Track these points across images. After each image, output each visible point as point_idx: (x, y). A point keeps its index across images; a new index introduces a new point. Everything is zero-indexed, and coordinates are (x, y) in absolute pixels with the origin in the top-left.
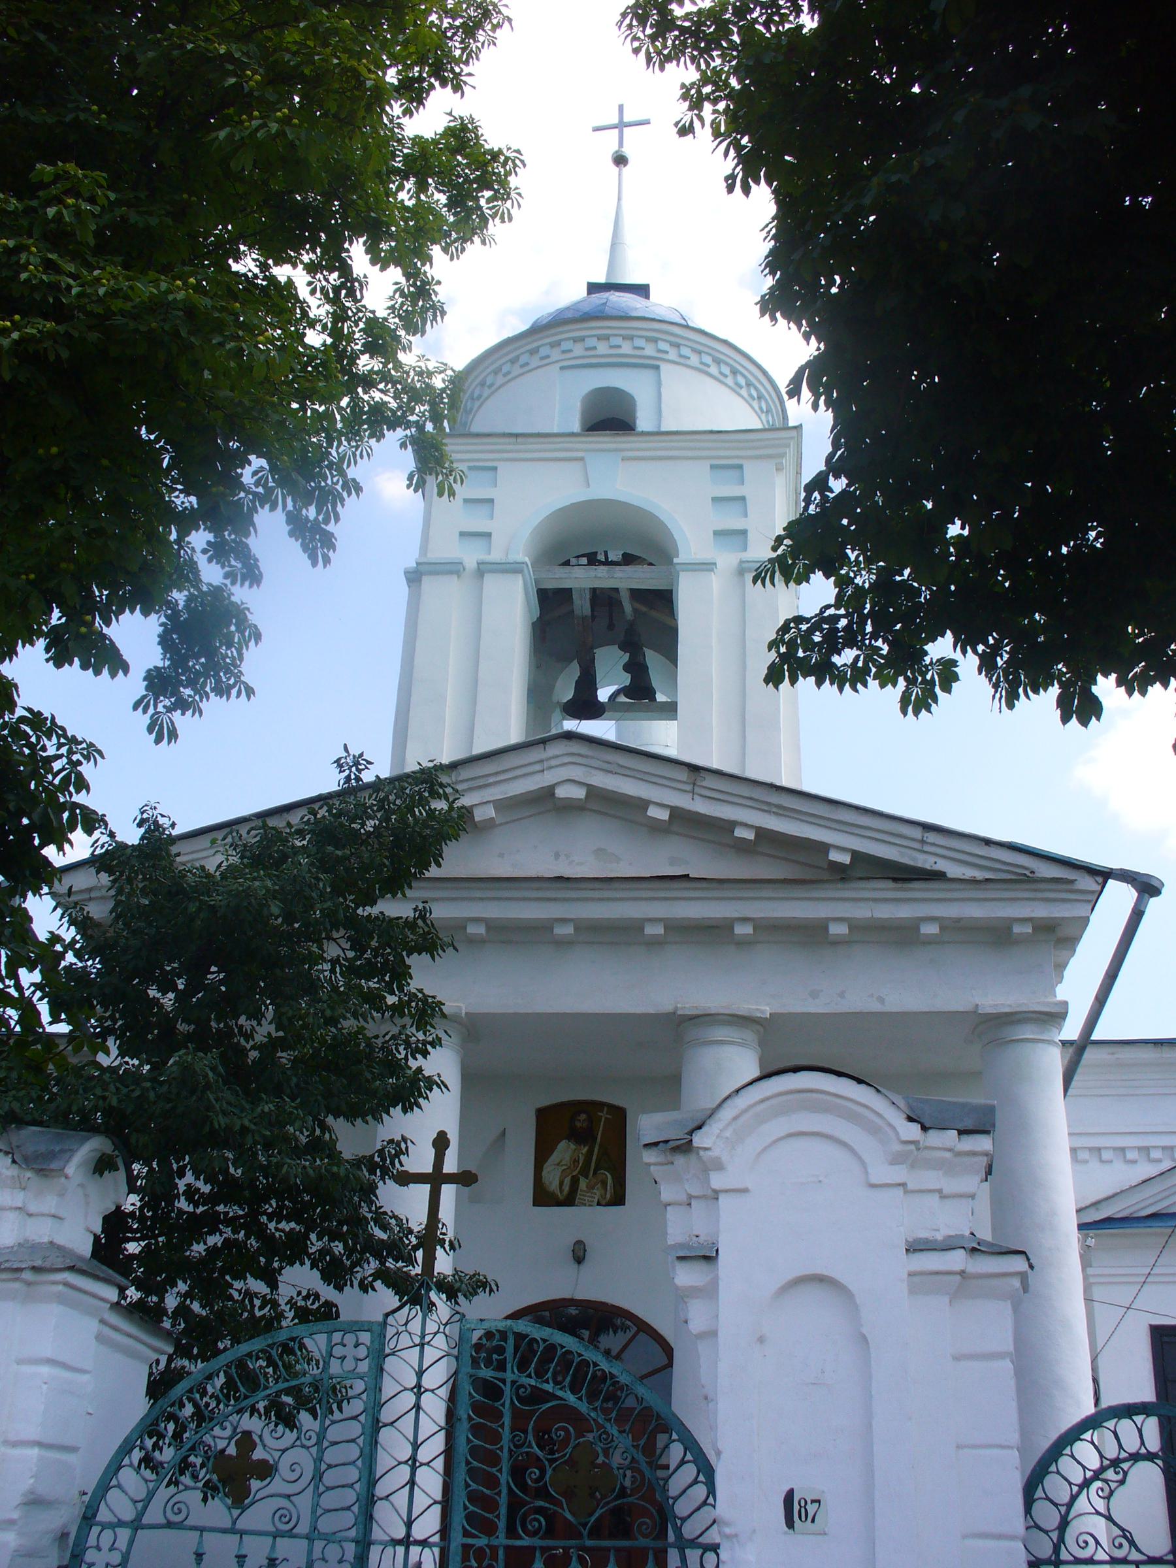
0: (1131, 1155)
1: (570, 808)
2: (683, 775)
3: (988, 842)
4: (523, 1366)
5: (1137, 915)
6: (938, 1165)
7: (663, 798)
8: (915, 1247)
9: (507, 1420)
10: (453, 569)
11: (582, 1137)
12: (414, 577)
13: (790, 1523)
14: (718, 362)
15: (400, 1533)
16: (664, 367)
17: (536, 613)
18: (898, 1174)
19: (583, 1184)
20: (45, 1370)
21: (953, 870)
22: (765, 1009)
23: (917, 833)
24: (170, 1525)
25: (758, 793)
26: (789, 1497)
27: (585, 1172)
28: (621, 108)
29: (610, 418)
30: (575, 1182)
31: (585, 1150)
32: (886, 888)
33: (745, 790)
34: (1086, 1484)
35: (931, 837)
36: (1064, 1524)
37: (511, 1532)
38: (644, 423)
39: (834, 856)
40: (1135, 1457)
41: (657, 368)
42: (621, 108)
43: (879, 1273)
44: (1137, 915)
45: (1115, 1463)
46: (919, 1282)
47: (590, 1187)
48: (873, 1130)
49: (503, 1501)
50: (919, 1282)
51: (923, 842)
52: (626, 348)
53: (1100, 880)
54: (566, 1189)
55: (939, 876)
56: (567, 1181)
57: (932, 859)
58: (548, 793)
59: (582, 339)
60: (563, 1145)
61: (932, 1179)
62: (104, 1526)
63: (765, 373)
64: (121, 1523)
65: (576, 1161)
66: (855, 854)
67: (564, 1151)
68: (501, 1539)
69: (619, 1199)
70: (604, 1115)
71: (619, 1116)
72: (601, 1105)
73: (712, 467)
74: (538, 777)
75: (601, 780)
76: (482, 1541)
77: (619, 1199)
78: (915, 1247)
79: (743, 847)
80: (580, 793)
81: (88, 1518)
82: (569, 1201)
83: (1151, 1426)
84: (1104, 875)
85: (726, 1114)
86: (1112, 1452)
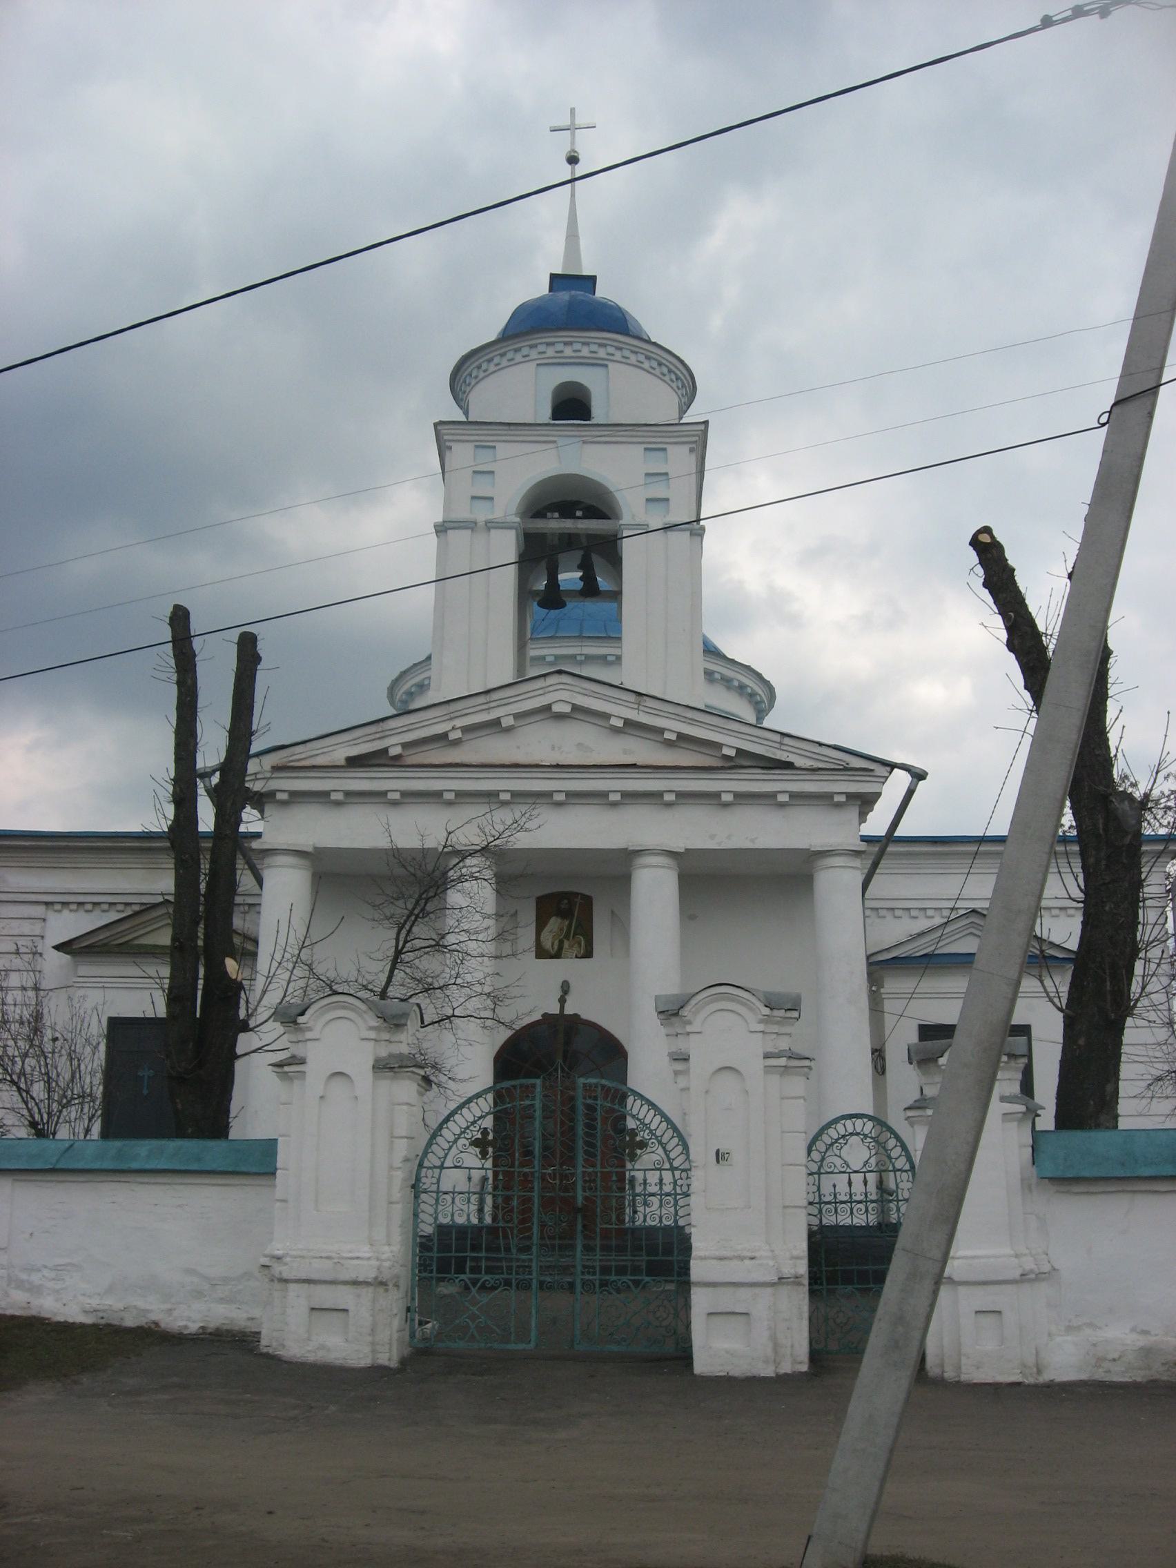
0: (913, 913)
1: (561, 717)
2: (632, 698)
3: (820, 744)
4: (605, 1098)
5: (910, 793)
6: (777, 1023)
7: (621, 711)
8: (767, 1056)
9: (599, 1120)
10: (470, 526)
11: (565, 914)
12: (441, 529)
13: (718, 1161)
14: (648, 358)
15: (438, 1163)
16: (611, 365)
17: (523, 548)
18: (761, 1027)
19: (566, 944)
20: (405, 1107)
21: (799, 762)
22: (679, 845)
23: (777, 738)
24: (456, 1167)
25: (679, 710)
26: (718, 1152)
27: (567, 937)
28: (573, 111)
29: (572, 406)
30: (561, 942)
31: (567, 923)
32: (758, 774)
33: (671, 709)
34: (832, 1144)
35: (787, 740)
36: (823, 1159)
37: (603, 1166)
38: (599, 413)
39: (726, 751)
40: (851, 1134)
41: (606, 366)
42: (573, 111)
43: (754, 1065)
44: (910, 793)
45: (844, 1136)
46: (768, 1069)
47: (571, 947)
48: (751, 1009)
49: (599, 1153)
50: (768, 1069)
51: (781, 743)
52: (585, 352)
53: (889, 769)
54: (556, 947)
55: (789, 766)
56: (556, 943)
57: (786, 754)
58: (548, 708)
59: (553, 344)
60: (553, 920)
61: (775, 1028)
62: (429, 1168)
63: (682, 362)
64: (435, 1167)
65: (561, 930)
66: (740, 752)
67: (554, 924)
68: (599, 1169)
69: (588, 954)
70: (578, 900)
71: (588, 902)
72: (577, 894)
73: (646, 449)
74: (542, 698)
75: (581, 701)
76: (591, 1170)
77: (588, 954)
78: (767, 1056)
79: (669, 744)
80: (567, 709)
81: (421, 1166)
82: (557, 955)
83: (670, 1223)
84: (892, 766)
85: (693, 1002)
86: (842, 1132)
